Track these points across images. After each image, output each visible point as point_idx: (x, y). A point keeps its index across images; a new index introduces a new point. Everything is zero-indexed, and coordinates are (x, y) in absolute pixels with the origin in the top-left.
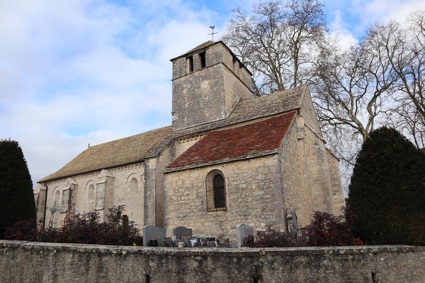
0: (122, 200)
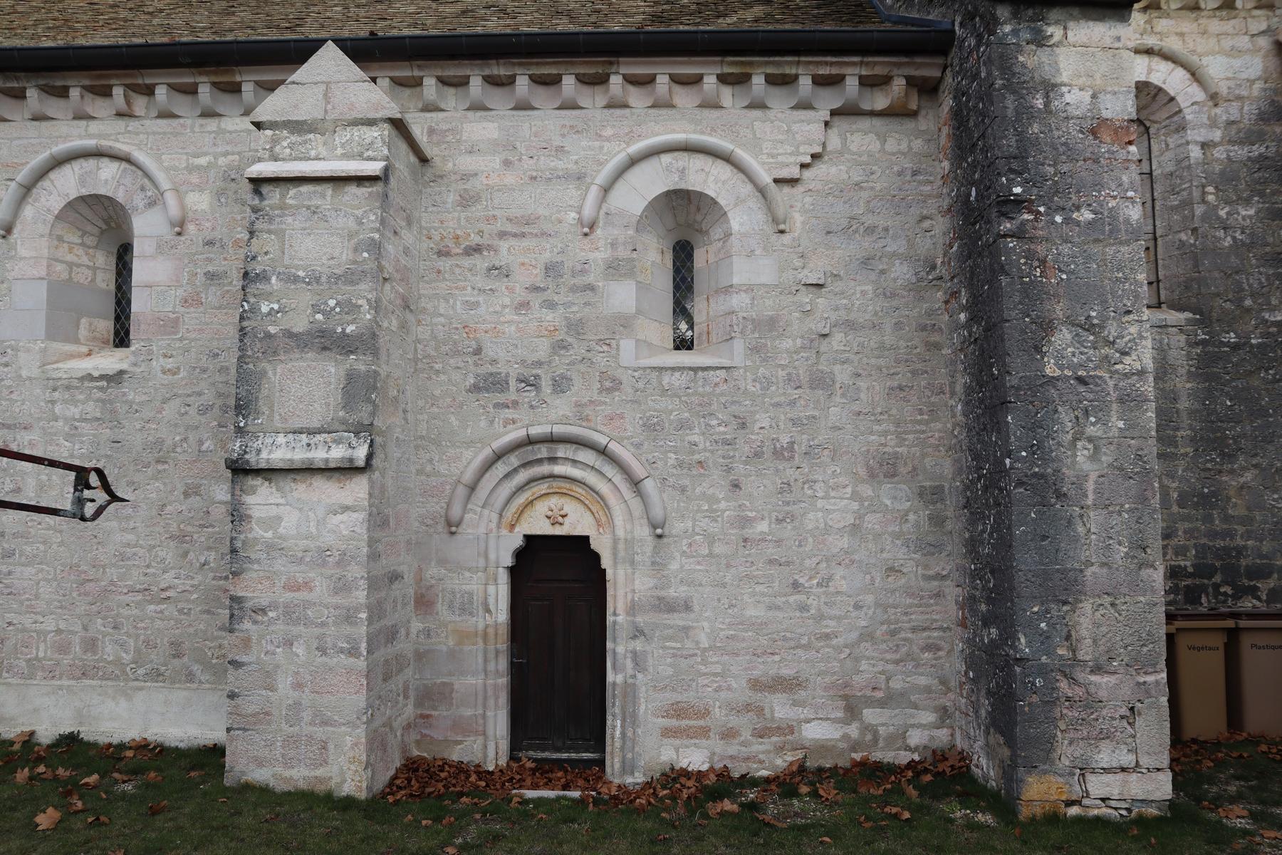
0: (530, 383)
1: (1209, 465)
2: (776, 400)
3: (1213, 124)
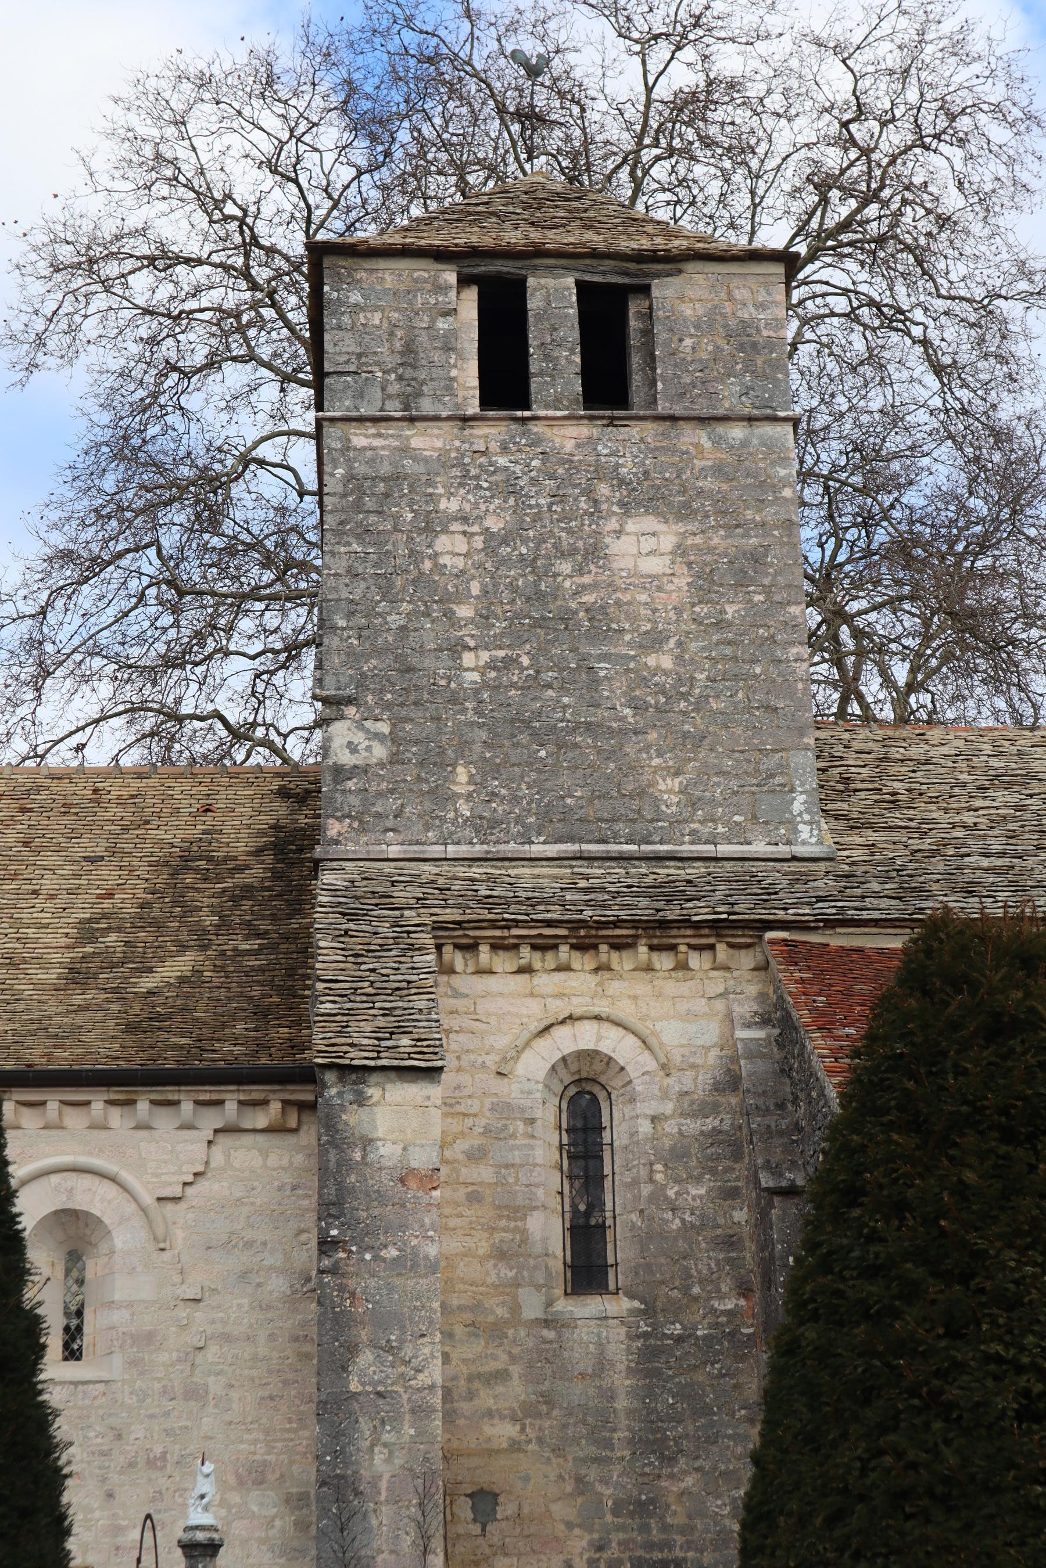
1: (647, 1470)
2: (151, 1411)
3: (665, 1095)
